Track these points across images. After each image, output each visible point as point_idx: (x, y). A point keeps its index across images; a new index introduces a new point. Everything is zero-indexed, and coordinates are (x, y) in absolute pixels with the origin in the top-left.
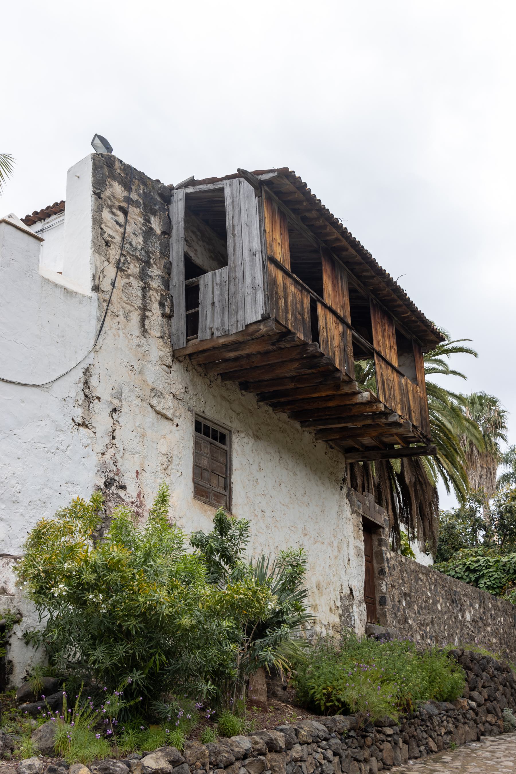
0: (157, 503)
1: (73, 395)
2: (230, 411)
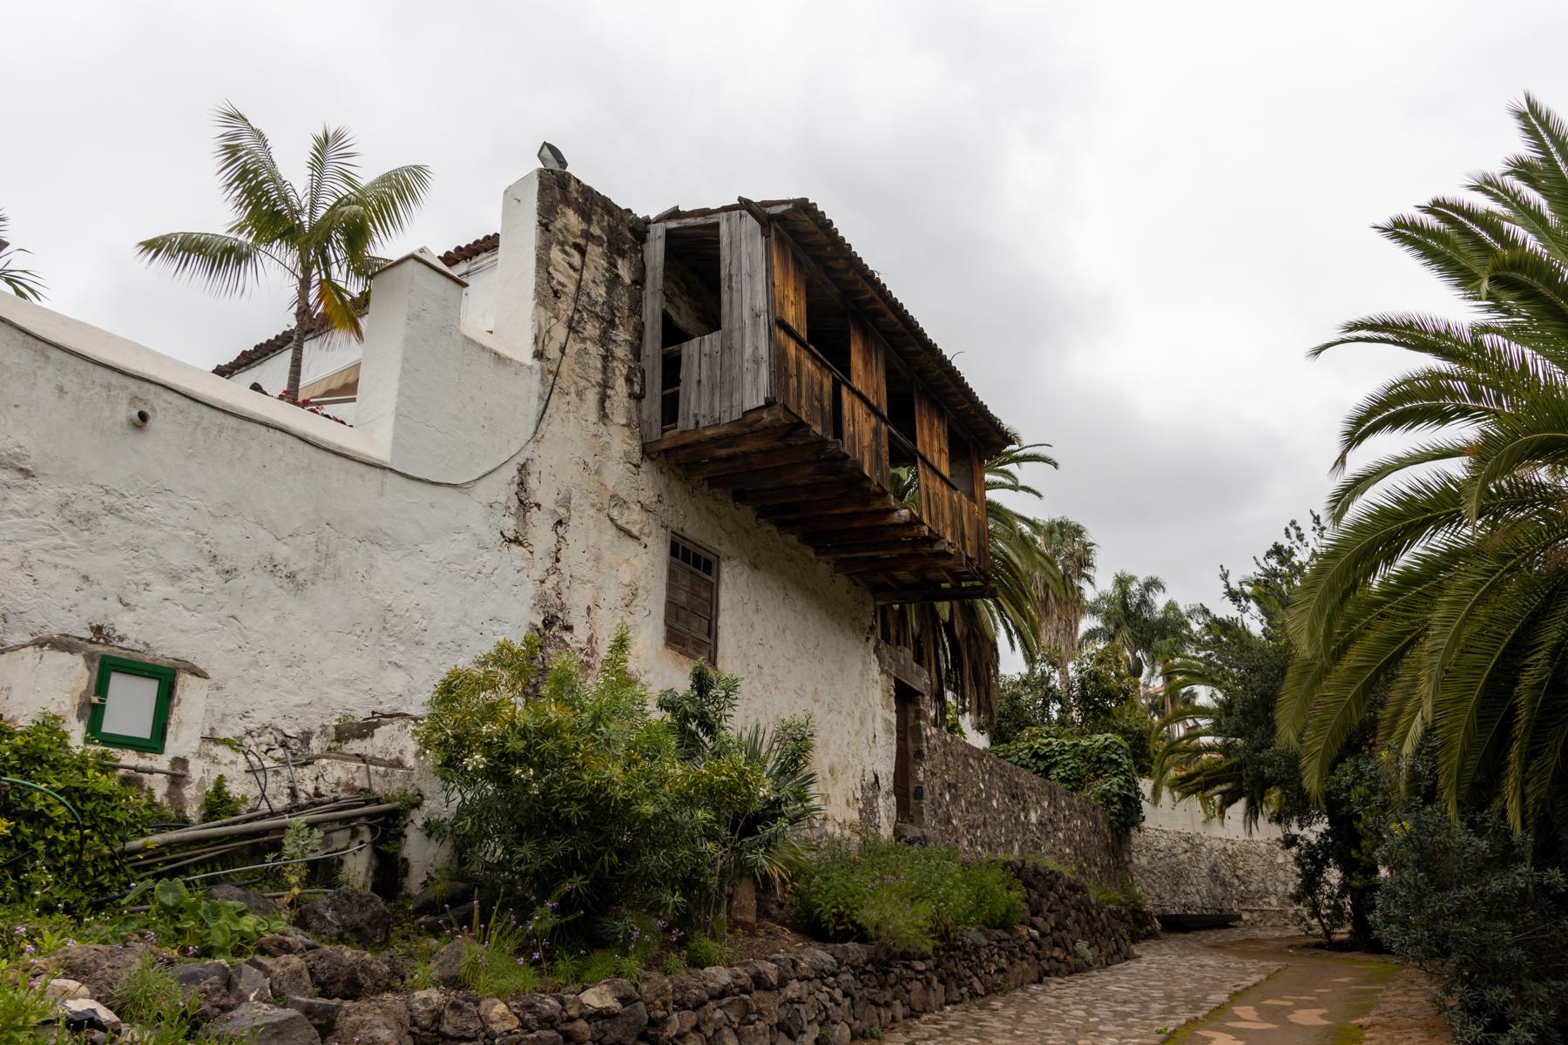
0: (613, 649)
1: (503, 499)
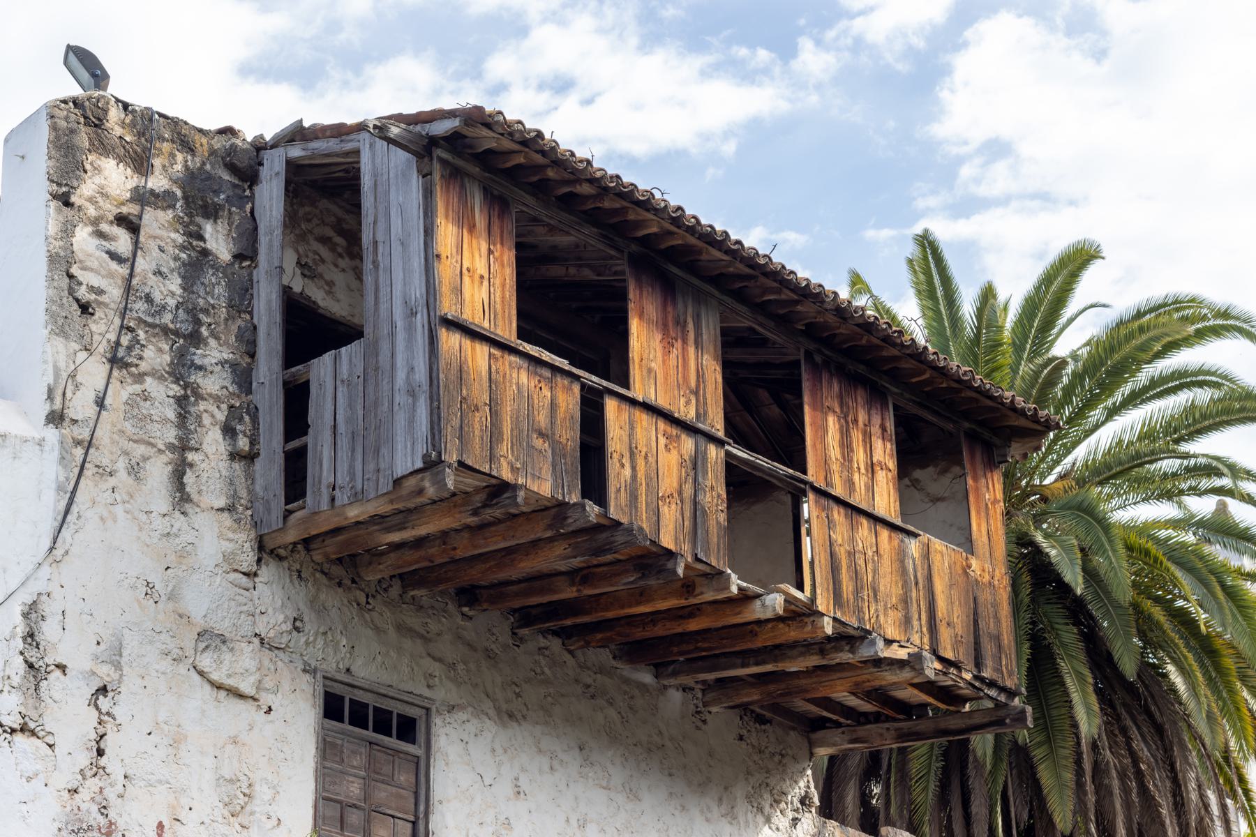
2: (427, 662)
